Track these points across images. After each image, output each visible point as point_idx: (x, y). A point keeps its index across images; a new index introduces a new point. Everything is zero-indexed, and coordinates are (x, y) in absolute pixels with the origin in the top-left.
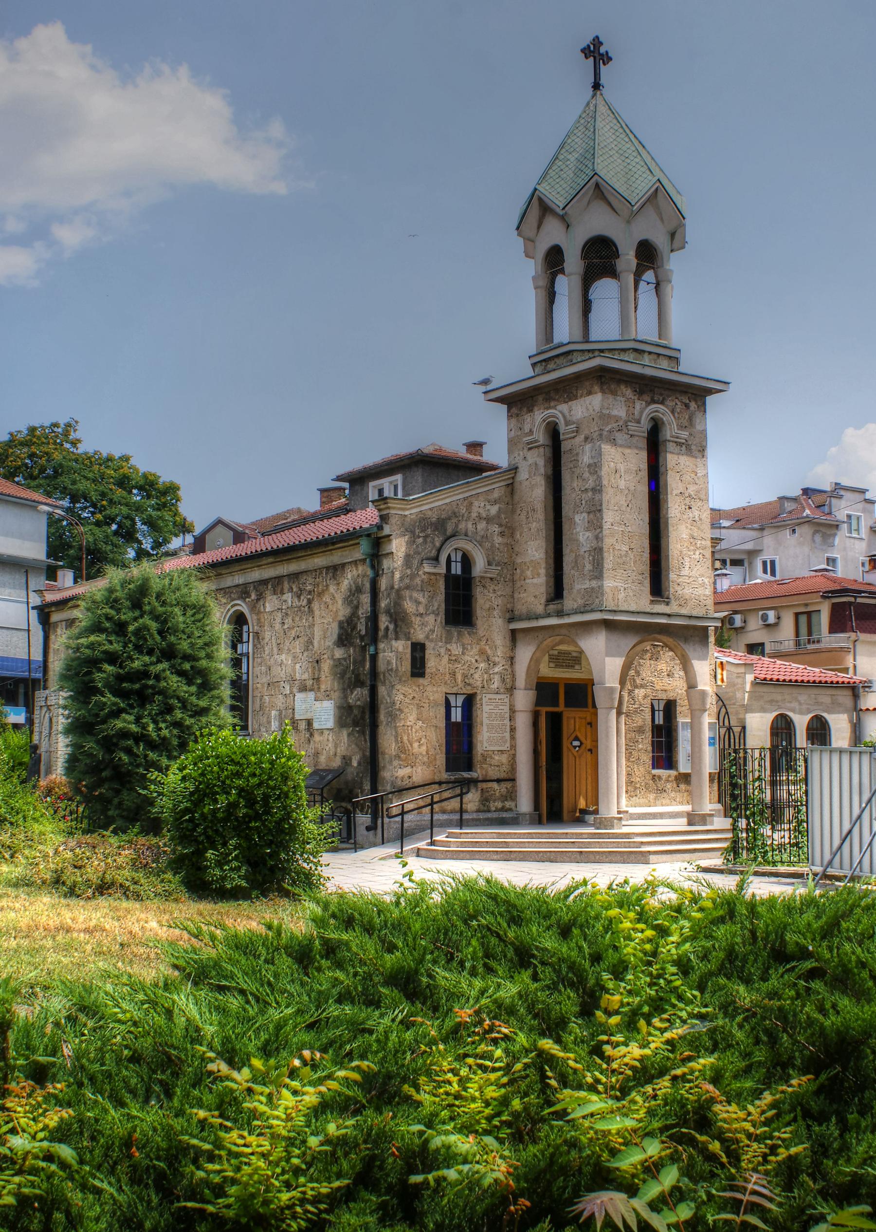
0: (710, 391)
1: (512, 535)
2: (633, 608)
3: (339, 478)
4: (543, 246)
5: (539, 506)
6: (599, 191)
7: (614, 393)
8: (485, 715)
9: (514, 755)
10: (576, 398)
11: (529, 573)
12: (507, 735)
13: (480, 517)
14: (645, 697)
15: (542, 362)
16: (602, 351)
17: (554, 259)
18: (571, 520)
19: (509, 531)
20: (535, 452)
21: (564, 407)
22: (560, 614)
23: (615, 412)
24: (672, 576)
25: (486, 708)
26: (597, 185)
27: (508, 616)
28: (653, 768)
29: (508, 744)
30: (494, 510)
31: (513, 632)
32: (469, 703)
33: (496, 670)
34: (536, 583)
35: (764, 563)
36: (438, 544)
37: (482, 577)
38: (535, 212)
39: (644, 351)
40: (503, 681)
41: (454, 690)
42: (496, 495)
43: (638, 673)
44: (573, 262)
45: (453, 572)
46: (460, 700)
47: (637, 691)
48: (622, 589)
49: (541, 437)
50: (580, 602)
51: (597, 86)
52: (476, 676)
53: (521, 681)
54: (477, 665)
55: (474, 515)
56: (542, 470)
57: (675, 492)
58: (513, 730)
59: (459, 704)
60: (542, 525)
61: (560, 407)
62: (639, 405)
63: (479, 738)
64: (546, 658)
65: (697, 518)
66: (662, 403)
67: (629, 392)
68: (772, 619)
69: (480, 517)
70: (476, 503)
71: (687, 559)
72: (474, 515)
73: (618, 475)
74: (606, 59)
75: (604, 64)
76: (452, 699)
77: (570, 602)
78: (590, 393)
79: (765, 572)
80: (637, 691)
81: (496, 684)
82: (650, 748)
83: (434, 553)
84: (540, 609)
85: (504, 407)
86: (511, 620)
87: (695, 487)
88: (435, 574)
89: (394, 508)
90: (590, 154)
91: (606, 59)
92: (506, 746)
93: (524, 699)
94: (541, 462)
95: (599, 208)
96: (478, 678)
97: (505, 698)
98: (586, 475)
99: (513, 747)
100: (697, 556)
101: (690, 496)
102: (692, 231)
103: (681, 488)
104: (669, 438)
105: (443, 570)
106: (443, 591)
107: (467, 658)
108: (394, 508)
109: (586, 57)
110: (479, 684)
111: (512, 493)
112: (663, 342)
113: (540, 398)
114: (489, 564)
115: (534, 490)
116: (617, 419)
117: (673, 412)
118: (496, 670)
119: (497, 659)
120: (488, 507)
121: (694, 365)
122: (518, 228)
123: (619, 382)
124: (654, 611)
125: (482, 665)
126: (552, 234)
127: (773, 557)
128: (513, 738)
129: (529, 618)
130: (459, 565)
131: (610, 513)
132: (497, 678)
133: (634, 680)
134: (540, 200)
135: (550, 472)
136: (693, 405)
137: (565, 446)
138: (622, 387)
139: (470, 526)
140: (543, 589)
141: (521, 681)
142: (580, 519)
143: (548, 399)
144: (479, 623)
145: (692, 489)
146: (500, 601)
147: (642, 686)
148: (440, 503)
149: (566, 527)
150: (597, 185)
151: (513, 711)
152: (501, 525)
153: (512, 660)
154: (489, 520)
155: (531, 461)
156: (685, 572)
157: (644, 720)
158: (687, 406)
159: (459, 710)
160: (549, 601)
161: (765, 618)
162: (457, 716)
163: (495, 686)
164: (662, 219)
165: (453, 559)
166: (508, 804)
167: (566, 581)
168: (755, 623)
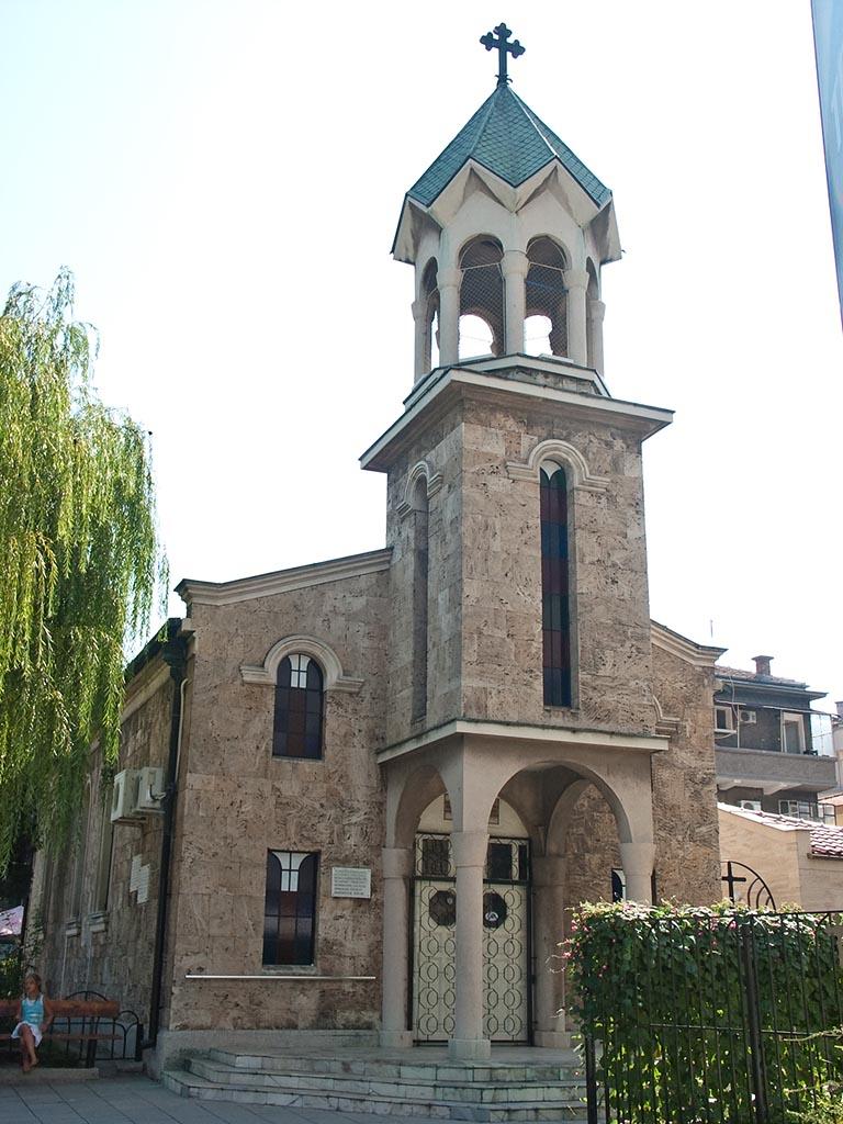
1: (385, 637)
2: (514, 717)
4: (423, 263)
5: (409, 592)
13: (335, 611)
14: (602, 865)
23: (487, 449)
24: (582, 676)
32: (312, 867)
33: (354, 819)
36: (267, 646)
37: (335, 691)
39: (537, 371)
40: (365, 834)
41: (283, 846)
42: (363, 584)
43: (590, 832)
46: (297, 861)
47: (587, 856)
50: (441, 713)
52: (321, 827)
54: (323, 811)
55: (327, 608)
57: (588, 560)
59: (296, 865)
62: (526, 440)
65: (627, 596)
67: (511, 423)
69: (335, 611)
70: (330, 594)
71: (607, 652)
72: (327, 608)
73: (489, 533)
74: (518, 50)
75: (515, 56)
76: (284, 860)
80: (587, 856)
81: (353, 839)
83: (258, 656)
86: (379, 752)
87: (623, 554)
88: (259, 685)
89: (196, 595)
91: (518, 50)
96: (323, 832)
101: (614, 565)
102: (628, 224)
103: (598, 554)
104: (576, 485)
105: (273, 678)
107: (306, 801)
108: (200, 596)
109: (488, 49)
110: (325, 837)
114: (346, 673)
116: (490, 458)
117: (584, 452)
118: (354, 819)
120: (349, 600)
122: (393, 251)
123: (495, 408)
130: (304, 676)
131: (475, 584)
132: (354, 830)
133: (584, 842)
139: (319, 621)
140: (409, 705)
144: (328, 753)
145: (617, 557)
146: (364, 725)
147: (596, 850)
148: (273, 592)
153: (380, 806)
156: (605, 671)
159: (295, 875)
162: (289, 883)
164: (569, 210)
166: (367, 1016)
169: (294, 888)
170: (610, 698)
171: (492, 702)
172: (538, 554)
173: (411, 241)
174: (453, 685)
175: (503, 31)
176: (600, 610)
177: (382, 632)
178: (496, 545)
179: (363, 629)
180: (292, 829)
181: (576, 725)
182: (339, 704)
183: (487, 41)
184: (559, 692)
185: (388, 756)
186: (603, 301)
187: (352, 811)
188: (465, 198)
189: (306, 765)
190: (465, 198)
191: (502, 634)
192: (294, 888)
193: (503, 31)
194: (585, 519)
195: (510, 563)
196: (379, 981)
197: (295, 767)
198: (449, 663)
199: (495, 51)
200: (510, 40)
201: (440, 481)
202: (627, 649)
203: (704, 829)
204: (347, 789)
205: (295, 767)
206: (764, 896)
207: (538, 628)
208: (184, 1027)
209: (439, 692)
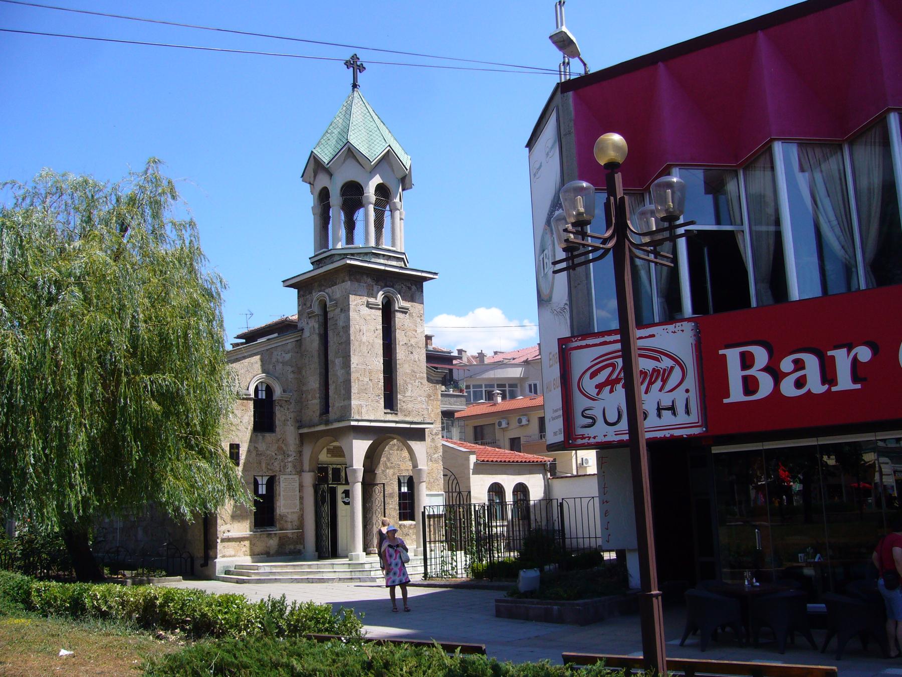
0: (426, 279)
2: (372, 418)
3: (239, 337)
4: (318, 188)
5: (316, 354)
6: (350, 153)
7: (359, 281)
8: (282, 489)
9: (302, 515)
10: (336, 284)
11: (310, 397)
12: (298, 502)
13: (277, 361)
14: (394, 474)
15: (317, 262)
16: (352, 254)
17: (324, 196)
18: (333, 362)
19: (299, 370)
20: (313, 320)
21: (329, 290)
22: (327, 423)
24: (399, 396)
25: (282, 485)
26: (349, 149)
27: (297, 425)
28: (400, 520)
29: (298, 507)
30: (288, 357)
31: (302, 436)
32: (271, 483)
33: (290, 460)
34: (315, 404)
35: (530, 386)
36: (249, 380)
38: (312, 165)
40: (295, 467)
41: (260, 474)
42: (289, 347)
43: (389, 460)
44: (336, 199)
45: (260, 397)
46: (265, 480)
48: (366, 407)
49: (316, 309)
51: (355, 86)
52: (276, 464)
53: (306, 466)
55: (274, 360)
56: (317, 331)
57: (401, 343)
58: (301, 498)
59: (265, 482)
60: (317, 366)
61: (327, 291)
63: (278, 504)
64: (325, 450)
66: (392, 287)
67: (369, 280)
68: (524, 422)
69: (277, 361)
70: (275, 353)
72: (274, 360)
74: (361, 68)
77: (332, 415)
78: (343, 281)
79: (531, 391)
81: (290, 468)
82: (397, 508)
84: (316, 418)
85: (294, 292)
86: (299, 428)
90: (346, 130)
91: (361, 68)
92: (297, 509)
93: (309, 479)
94: (316, 326)
95: (350, 163)
97: (296, 477)
98: (341, 333)
99: (302, 509)
100: (417, 384)
103: (405, 340)
106: (252, 410)
107: (268, 452)
110: (277, 469)
111: (300, 346)
112: (394, 249)
113: (316, 284)
114: (284, 391)
115: (313, 342)
118: (290, 460)
119: (290, 453)
121: (416, 264)
124: (387, 419)
125: (280, 457)
126: (323, 181)
127: (535, 382)
128: (301, 503)
129: (310, 426)
130: (264, 393)
132: (290, 465)
134: (314, 157)
135: (322, 332)
136: (414, 288)
137: (330, 315)
138: (365, 277)
139: (271, 367)
140: (318, 407)
141: (306, 466)
142: (338, 362)
143: (320, 285)
144: (278, 429)
146: (292, 415)
147: (391, 468)
149: (330, 367)
150: (349, 149)
151: (301, 487)
152: (292, 367)
153: (300, 453)
154: (284, 363)
155: (311, 325)
156: (408, 394)
157: (393, 489)
158: (410, 288)
159: (264, 486)
160: (321, 415)
161: (520, 421)
162: (262, 490)
163: (289, 470)
165: (260, 388)
167: (330, 401)
168: (514, 423)
169: (264, 492)
170: (410, 406)
171: (364, 410)
172: (381, 342)
173: (313, 174)
174: (346, 403)
175: (355, 57)
176: (406, 366)
177: (299, 370)
178: (364, 339)
179: (290, 369)
180: (264, 466)
181: (397, 419)
182: (281, 406)
183: (348, 64)
184: (390, 402)
185: (305, 430)
186: (472, 351)
187: (288, 456)
188: (345, 160)
189: (268, 436)
190: (345, 160)
191: (367, 379)
192: (264, 492)
193: (355, 57)
194: (400, 324)
195: (370, 347)
196: (303, 532)
197: (263, 437)
198: (343, 392)
199: (352, 69)
200: (359, 63)
201: (336, 305)
202: (417, 384)
203: (436, 456)
204: (286, 445)
205: (263, 437)
206: (455, 482)
207: (381, 376)
208: (224, 556)
209: (337, 405)
